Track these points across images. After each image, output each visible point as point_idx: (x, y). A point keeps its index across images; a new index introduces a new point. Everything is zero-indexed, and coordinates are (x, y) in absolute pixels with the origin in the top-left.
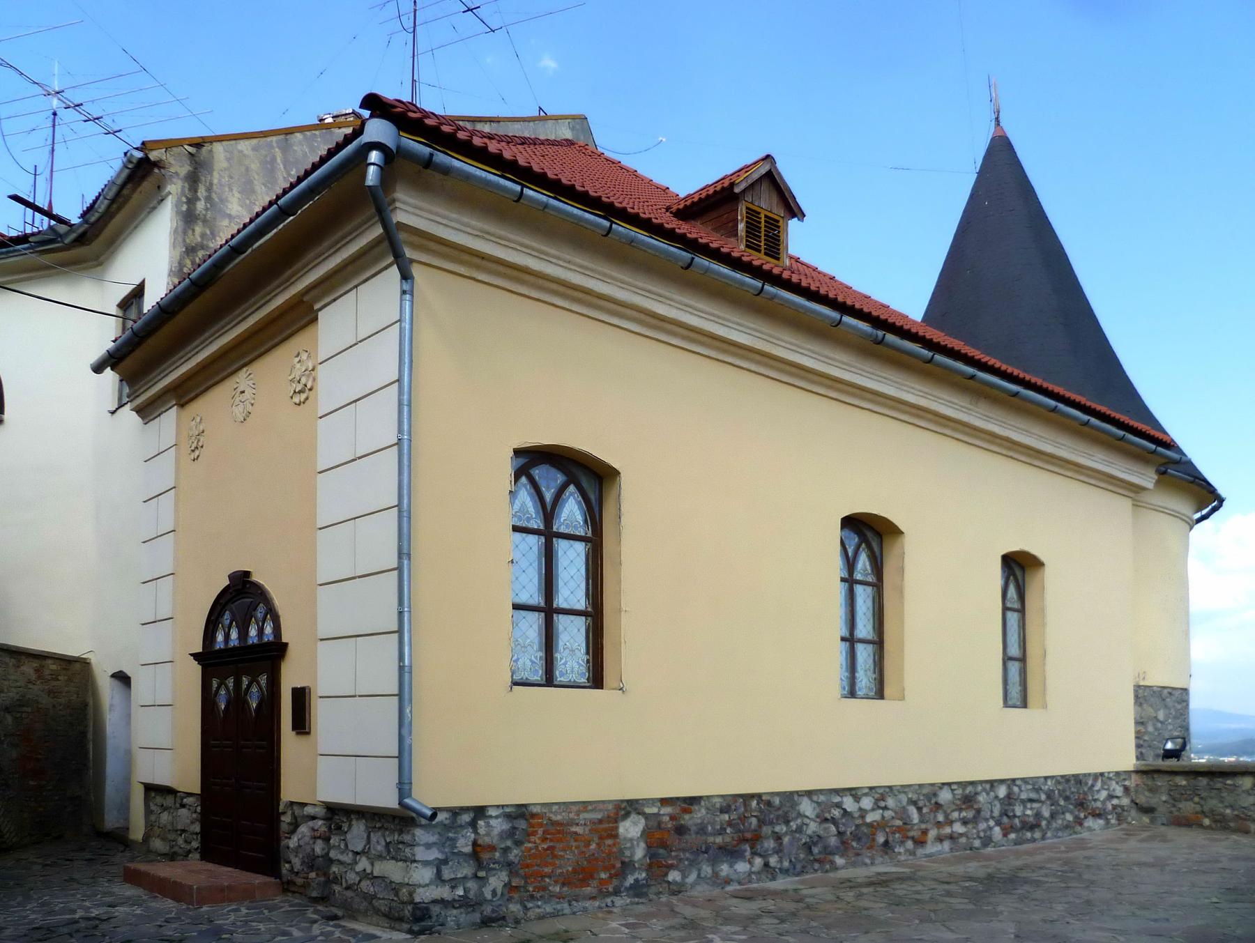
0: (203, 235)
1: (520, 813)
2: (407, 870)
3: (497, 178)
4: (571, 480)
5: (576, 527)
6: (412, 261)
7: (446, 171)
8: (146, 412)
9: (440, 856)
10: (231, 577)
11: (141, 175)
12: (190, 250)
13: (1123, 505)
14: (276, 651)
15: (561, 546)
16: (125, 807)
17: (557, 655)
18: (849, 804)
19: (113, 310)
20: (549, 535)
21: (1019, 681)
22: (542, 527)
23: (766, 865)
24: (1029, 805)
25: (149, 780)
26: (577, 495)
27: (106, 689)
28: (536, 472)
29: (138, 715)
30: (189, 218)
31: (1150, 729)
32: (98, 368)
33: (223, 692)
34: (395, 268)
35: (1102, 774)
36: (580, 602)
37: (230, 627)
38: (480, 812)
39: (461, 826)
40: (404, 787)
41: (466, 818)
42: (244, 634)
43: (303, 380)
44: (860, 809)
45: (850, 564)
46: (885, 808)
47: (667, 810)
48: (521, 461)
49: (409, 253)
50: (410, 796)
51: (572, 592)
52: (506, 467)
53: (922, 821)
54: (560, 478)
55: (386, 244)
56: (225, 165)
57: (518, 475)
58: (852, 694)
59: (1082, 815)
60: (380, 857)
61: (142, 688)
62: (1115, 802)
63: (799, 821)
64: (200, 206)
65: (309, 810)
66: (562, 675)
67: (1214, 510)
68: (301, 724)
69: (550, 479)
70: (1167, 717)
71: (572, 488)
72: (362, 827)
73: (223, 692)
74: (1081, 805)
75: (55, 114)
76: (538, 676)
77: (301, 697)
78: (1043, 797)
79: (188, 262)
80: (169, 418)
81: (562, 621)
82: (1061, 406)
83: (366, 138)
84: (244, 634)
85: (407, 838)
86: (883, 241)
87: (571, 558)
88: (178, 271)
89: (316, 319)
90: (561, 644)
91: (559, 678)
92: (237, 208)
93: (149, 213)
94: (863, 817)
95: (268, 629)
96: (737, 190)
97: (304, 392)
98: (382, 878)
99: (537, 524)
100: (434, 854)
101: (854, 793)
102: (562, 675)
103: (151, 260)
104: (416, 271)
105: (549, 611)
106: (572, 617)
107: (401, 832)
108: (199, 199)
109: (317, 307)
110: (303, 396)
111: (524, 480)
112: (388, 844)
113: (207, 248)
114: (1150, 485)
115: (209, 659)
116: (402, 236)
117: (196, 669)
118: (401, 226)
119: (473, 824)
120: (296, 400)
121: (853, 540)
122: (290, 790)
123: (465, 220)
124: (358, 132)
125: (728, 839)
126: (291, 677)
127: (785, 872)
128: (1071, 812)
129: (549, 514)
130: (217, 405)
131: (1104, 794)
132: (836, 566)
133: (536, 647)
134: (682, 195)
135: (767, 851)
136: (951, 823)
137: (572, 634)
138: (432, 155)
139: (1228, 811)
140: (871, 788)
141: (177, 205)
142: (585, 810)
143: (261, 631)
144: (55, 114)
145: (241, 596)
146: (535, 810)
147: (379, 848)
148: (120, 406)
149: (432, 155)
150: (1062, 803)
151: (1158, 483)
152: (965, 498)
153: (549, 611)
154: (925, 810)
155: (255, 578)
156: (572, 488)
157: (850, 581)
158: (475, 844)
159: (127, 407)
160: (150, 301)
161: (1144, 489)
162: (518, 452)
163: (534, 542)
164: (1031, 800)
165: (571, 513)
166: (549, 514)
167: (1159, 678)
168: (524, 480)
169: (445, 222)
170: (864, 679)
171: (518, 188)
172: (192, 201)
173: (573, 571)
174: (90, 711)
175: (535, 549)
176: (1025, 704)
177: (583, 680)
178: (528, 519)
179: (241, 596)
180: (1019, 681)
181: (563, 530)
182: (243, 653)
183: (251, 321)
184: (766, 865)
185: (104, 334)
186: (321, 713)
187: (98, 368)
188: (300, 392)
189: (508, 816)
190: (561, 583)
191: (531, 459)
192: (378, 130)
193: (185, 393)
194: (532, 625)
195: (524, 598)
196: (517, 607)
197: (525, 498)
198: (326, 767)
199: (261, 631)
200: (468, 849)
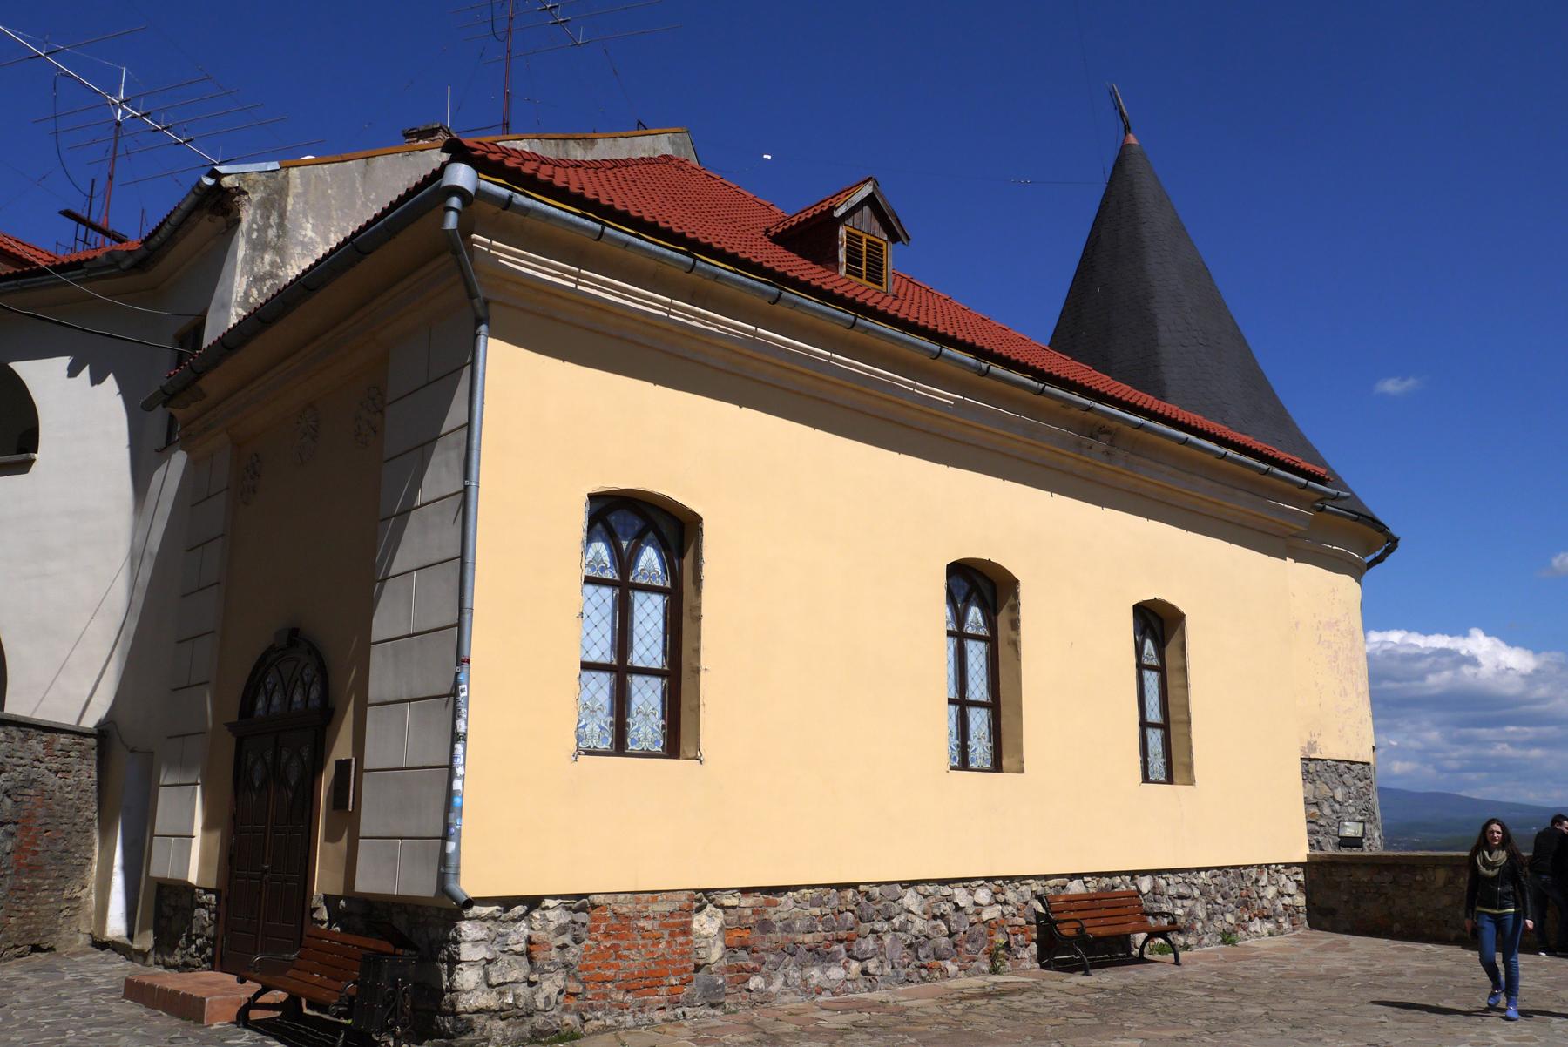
0: (273, 264)
21: (1166, 747)
22: (668, 585)
24: (1179, 902)
28: (612, 518)
31: (1327, 811)
35: (1268, 866)
40: (445, 866)
44: (975, 904)
45: (959, 617)
48: (599, 505)
51: (648, 648)
54: (638, 524)
59: (1246, 917)
62: (1287, 900)
63: (902, 918)
64: (272, 233)
66: (634, 742)
67: (1389, 551)
70: (1349, 795)
71: (651, 535)
74: (1245, 904)
78: (1197, 893)
79: (255, 292)
87: (649, 613)
90: (634, 707)
106: (594, 674)
128: (1232, 912)
129: (625, 562)
131: (1271, 892)
135: (865, 952)
137: (647, 696)
139: (1421, 914)
142: (655, 901)
146: (597, 900)
150: (1220, 901)
156: (651, 535)
158: (529, 941)
164: (1181, 897)
166: (625, 562)
171: (598, 227)
172: (263, 230)
173: (649, 625)
175: (609, 602)
178: (603, 569)
180: (1166, 747)
181: (639, 580)
190: (636, 639)
195: (595, 656)
196: (586, 666)
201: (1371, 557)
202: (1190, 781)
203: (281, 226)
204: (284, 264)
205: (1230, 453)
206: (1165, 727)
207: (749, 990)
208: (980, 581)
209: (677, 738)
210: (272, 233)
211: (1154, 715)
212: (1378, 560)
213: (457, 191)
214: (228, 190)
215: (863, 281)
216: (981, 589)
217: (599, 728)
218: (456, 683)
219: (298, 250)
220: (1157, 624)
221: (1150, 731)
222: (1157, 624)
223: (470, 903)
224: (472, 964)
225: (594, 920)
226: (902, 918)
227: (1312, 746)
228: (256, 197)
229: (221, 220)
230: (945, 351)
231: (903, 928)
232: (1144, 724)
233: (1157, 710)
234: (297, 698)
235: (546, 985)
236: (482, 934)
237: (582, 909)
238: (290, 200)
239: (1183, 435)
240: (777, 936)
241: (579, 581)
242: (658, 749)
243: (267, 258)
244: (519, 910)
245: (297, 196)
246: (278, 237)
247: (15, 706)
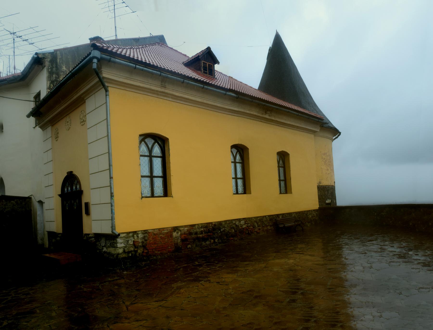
0: (56, 77)
1: (145, 232)
2: (115, 250)
3: (129, 63)
4: (156, 141)
5: (145, 153)
6: (108, 87)
7: (115, 62)
8: (43, 127)
9: (124, 246)
10: (68, 173)
11: (38, 61)
12: (52, 82)
13: (312, 136)
14: (80, 193)
15: (154, 159)
16: (42, 239)
17: (154, 189)
18: (237, 223)
19: (32, 99)
20: (151, 157)
21: (285, 186)
23: (214, 242)
25: (49, 230)
26: (158, 145)
27: (37, 206)
29: (46, 212)
30: (51, 73)
32: (28, 116)
33: (75, 204)
34: (103, 89)
36: (160, 174)
37: (68, 186)
38: (135, 233)
39: (130, 237)
40: (113, 227)
41: (131, 235)
42: (72, 189)
43: (83, 119)
45: (235, 158)
46: (248, 224)
47: (186, 229)
48: (142, 137)
49: (106, 84)
50: (115, 229)
51: (158, 170)
52: (137, 140)
53: (258, 226)
55: (100, 83)
56: (60, 57)
57: (140, 142)
58: (237, 193)
60: (109, 247)
61: (46, 206)
64: (54, 69)
65: (90, 235)
66: (156, 194)
67: (339, 135)
68: (88, 213)
69: (150, 142)
71: (156, 144)
72: (104, 239)
73: (75, 204)
75: (14, 39)
76: (149, 195)
77: (87, 205)
79: (52, 85)
80: (49, 129)
81: (155, 180)
82: (290, 111)
83: (91, 56)
84: (72, 189)
85: (115, 241)
86: (245, 68)
87: (157, 163)
88: (49, 88)
89: (85, 102)
90: (155, 186)
91: (155, 195)
92: (65, 70)
93: (40, 72)
94: (242, 227)
95: (78, 187)
96: (200, 58)
97: (83, 122)
98: (110, 253)
99: (147, 154)
100: (123, 245)
101: (239, 220)
102: (156, 194)
103: (42, 86)
104: (109, 89)
105: (152, 177)
107: (114, 240)
108: (54, 67)
109: (85, 99)
110: (83, 123)
111: (143, 142)
112: (111, 243)
113: (57, 81)
114: (318, 130)
115: (63, 195)
116: (105, 80)
117: (60, 199)
118: (104, 78)
119: (133, 236)
120: (82, 124)
121: (235, 151)
122: (86, 231)
123: (121, 74)
124: (90, 53)
125: (203, 235)
126: (85, 199)
127: (219, 243)
129: (150, 151)
130: (62, 125)
132: (231, 158)
133: (149, 187)
134: (190, 57)
136: (267, 226)
137: (158, 183)
138: (110, 59)
140: (243, 219)
141: (48, 69)
142: (164, 230)
143: (76, 188)
144: (14, 39)
145: (71, 179)
146: (149, 231)
147: (109, 245)
148: (36, 126)
149: (110, 59)
151: (320, 130)
152: (265, 139)
153: (152, 177)
154: (259, 223)
155: (74, 173)
157: (235, 162)
158: (134, 242)
159: (38, 126)
160: (43, 96)
161: (317, 132)
162: (140, 135)
163: (147, 159)
165: (157, 150)
166: (150, 151)
167: (325, 183)
168: (143, 142)
169: (144, 54)
170: (240, 189)
171: (134, 65)
172: (52, 68)
174: (33, 212)
175: (147, 161)
176: (286, 192)
177: (162, 195)
178: (145, 153)
179: (71, 179)
180: (285, 186)
181: (154, 155)
182: (72, 193)
183: (51, 116)
184: (214, 242)
185: (32, 106)
186: (92, 209)
187: (28, 116)
188: (83, 122)
189: (143, 233)
190: (155, 169)
191: (144, 137)
192: (96, 53)
193: (53, 122)
194: (147, 181)
195: (145, 174)
196: (142, 177)
197: (144, 148)
198: (95, 224)
199: (76, 188)
200: (132, 243)
201: (335, 137)
202: (291, 193)
203: (56, 67)
204: (59, 78)
205: (299, 114)
206: (285, 180)
207: (188, 248)
208: (240, 150)
209: (166, 193)
210: (54, 69)
211: (282, 178)
212: (336, 138)
213: (94, 57)
214: (41, 58)
215: (208, 75)
216: (241, 151)
217: (147, 192)
218: (110, 183)
219: (62, 73)
220: (283, 158)
221: (281, 182)
222: (283, 158)
223: (119, 235)
224: (120, 248)
225: (149, 235)
226: (224, 229)
227: (320, 183)
228: (49, 60)
229: (40, 66)
230: (227, 93)
231: (224, 231)
232: (280, 180)
233: (283, 177)
234: (74, 188)
235: (139, 251)
236: (122, 241)
237: (146, 233)
238: (58, 60)
239: (288, 110)
240: (193, 236)
241: (138, 156)
242: (162, 195)
243: (54, 76)
244: (131, 235)
245: (60, 59)
246: (56, 70)
247: (9, 192)
